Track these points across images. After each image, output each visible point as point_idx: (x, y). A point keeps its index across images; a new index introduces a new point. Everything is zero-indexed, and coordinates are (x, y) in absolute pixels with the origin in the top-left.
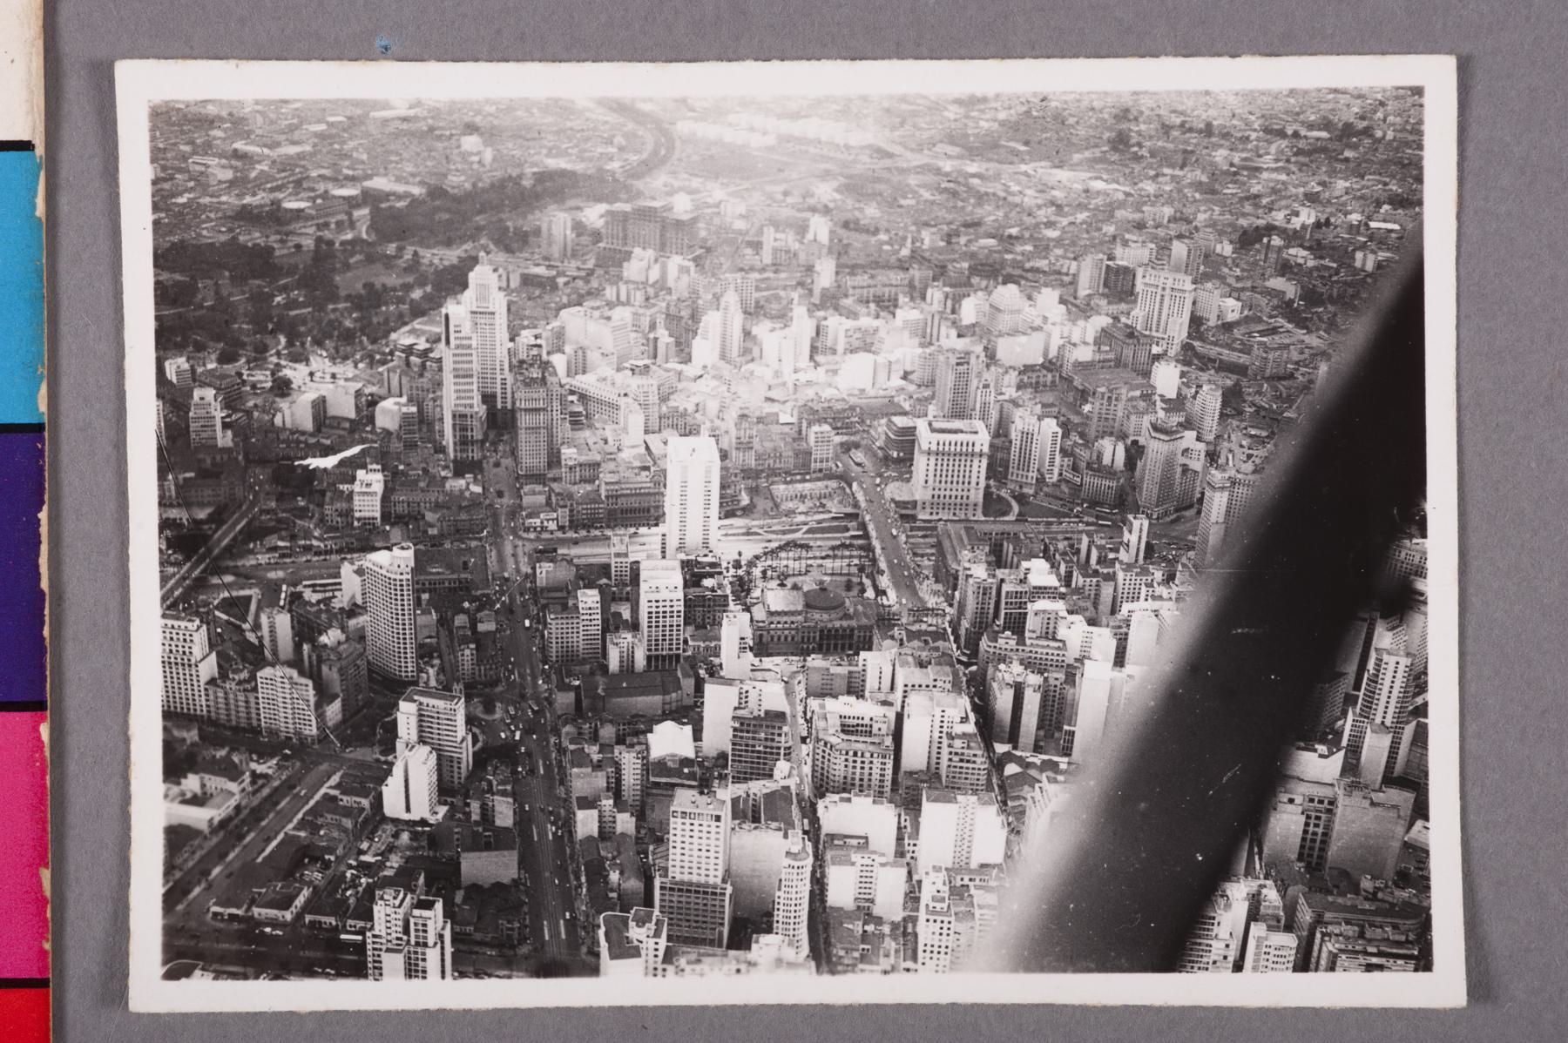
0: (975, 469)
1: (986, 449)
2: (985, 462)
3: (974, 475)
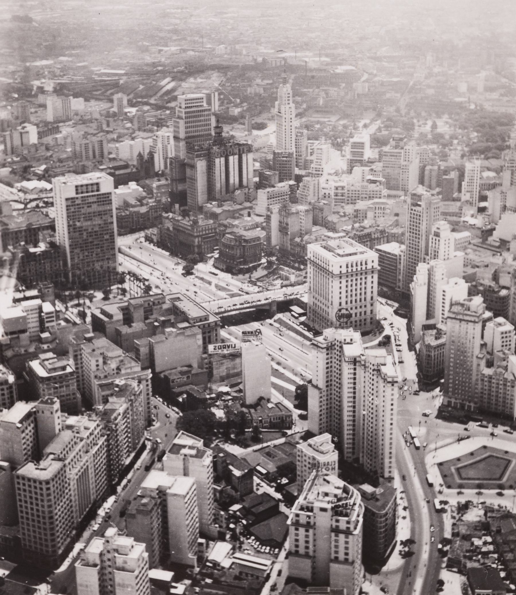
0: (369, 285)
2: (376, 276)
3: (369, 290)
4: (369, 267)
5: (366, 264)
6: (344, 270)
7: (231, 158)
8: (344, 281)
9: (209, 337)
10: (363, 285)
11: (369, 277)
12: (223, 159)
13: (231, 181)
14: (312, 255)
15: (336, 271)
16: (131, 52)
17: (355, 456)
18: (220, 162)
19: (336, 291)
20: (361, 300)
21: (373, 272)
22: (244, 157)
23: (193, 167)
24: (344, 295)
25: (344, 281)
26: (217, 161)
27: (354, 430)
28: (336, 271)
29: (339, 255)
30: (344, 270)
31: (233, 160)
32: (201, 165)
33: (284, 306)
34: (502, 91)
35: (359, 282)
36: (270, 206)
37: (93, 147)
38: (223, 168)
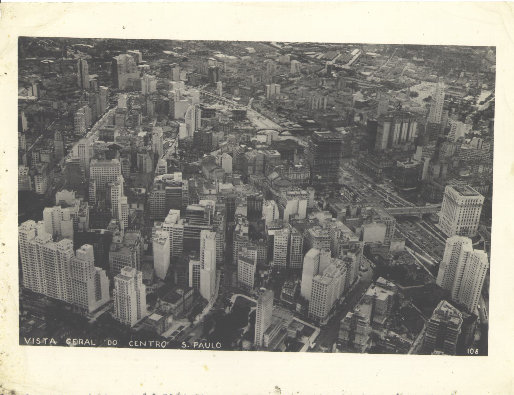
0: (476, 213)
1: (482, 203)
2: (481, 208)
3: (476, 215)
4: (478, 203)
5: (477, 201)
6: (464, 204)
7: (404, 124)
8: (463, 209)
9: (389, 228)
10: (473, 213)
11: (477, 208)
12: (400, 124)
13: (402, 138)
14: (447, 192)
15: (460, 204)
16: (428, 147)
17: (457, 299)
18: (397, 126)
19: (458, 213)
20: (470, 220)
21: (479, 206)
22: (411, 125)
23: (382, 127)
24: (462, 216)
25: (463, 209)
26: (396, 125)
27: (459, 289)
28: (460, 204)
29: (463, 195)
30: (464, 204)
31: (405, 126)
32: (387, 126)
33: (263, 336)
34: (464, 193)
35: (471, 210)
36: (425, 158)
37: (319, 101)
38: (399, 130)
